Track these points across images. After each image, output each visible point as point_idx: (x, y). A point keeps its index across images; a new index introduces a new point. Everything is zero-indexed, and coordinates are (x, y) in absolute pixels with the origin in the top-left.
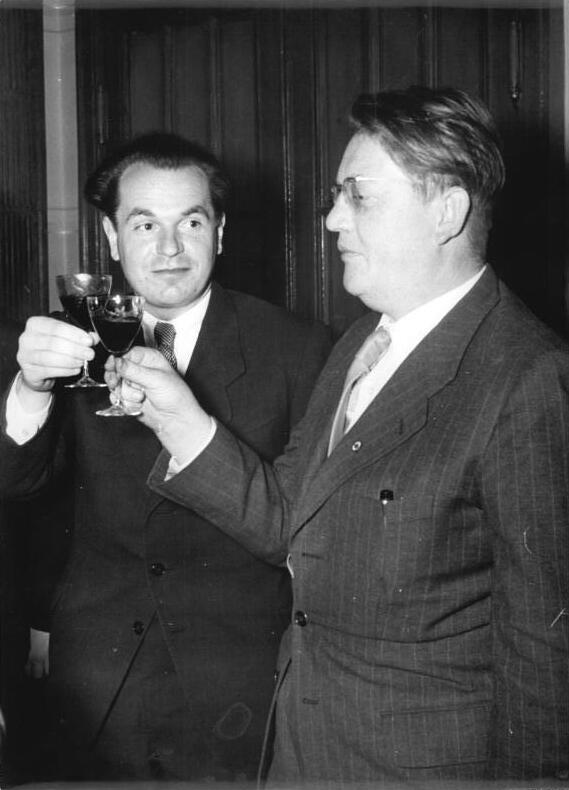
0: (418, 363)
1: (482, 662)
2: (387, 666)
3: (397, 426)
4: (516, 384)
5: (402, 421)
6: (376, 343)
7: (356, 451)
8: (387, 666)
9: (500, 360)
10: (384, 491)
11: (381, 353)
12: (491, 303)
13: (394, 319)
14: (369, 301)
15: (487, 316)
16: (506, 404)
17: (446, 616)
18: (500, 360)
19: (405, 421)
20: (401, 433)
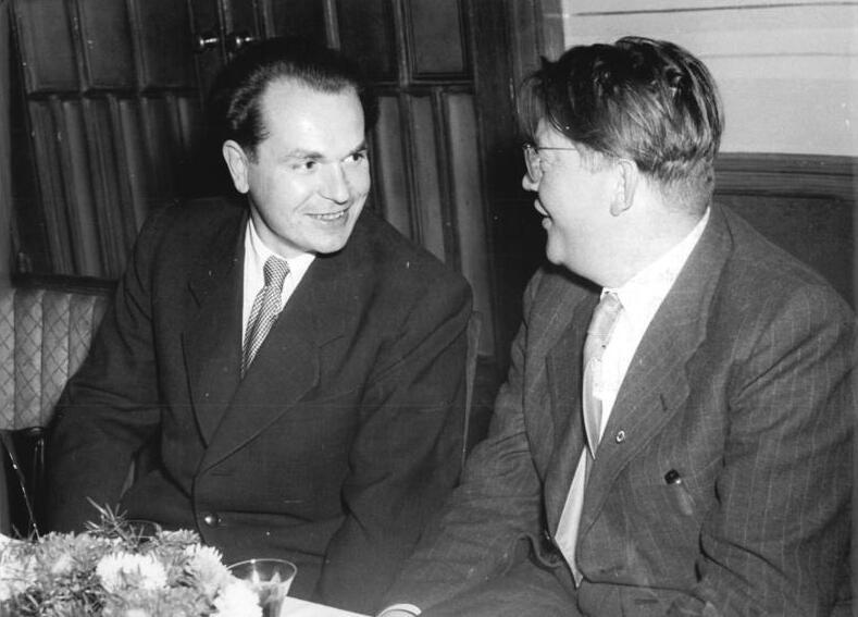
0: (662, 333)
1: (697, 292)
2: (765, 560)
3: (658, 403)
4: (767, 326)
5: (661, 397)
6: (607, 313)
7: (618, 431)
8: (765, 560)
9: (747, 306)
10: (669, 474)
11: (614, 320)
12: (725, 248)
13: (622, 283)
14: (599, 282)
15: (726, 265)
16: (758, 342)
17: (354, 342)
18: (747, 306)
19: (665, 396)
20: (665, 409)
